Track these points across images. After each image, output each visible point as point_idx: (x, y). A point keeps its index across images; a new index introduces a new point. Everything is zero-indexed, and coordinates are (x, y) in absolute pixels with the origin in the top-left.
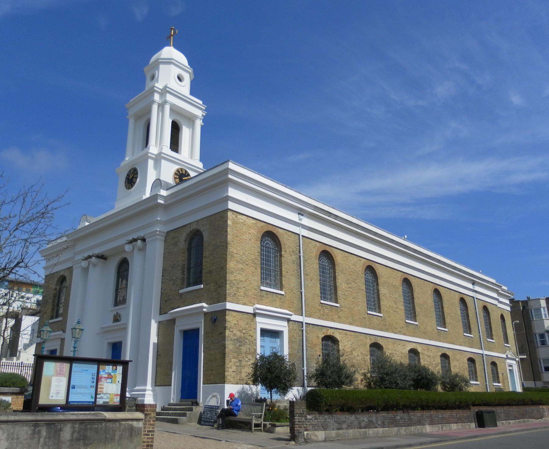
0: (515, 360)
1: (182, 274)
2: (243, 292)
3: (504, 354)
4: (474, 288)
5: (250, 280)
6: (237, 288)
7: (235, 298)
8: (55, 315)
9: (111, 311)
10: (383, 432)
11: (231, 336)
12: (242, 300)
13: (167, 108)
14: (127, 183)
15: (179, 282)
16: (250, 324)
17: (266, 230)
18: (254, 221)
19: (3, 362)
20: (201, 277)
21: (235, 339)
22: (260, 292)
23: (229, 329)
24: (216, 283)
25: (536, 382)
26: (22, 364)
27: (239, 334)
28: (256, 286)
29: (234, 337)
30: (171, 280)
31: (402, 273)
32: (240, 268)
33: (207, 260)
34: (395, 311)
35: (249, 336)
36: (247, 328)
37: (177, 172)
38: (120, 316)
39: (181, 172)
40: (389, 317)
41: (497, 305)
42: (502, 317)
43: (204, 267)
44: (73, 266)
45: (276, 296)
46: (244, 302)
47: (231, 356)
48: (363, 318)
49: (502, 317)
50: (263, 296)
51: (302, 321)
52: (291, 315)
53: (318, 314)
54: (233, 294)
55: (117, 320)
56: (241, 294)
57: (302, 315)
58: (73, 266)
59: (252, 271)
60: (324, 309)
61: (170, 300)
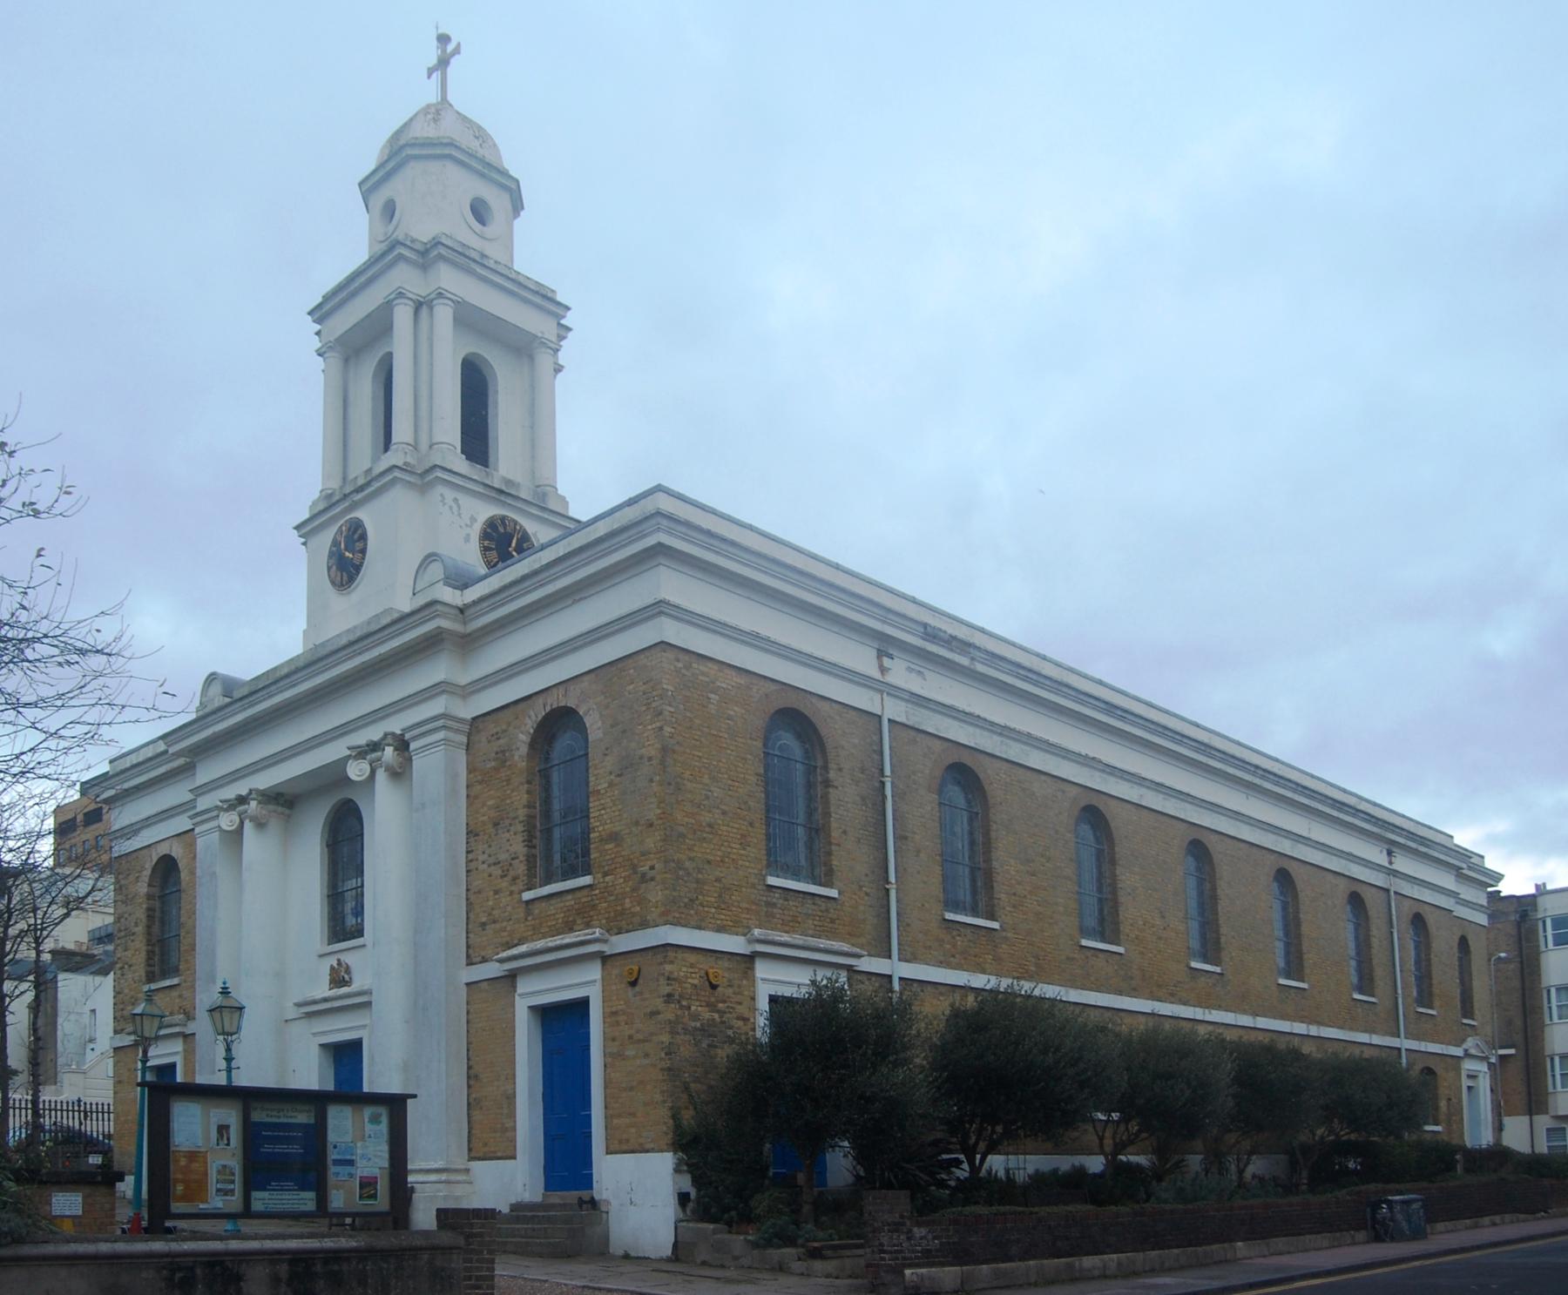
0: (1485, 1059)
1: (527, 846)
2: (716, 895)
3: (1459, 1046)
4: (1391, 863)
5: (734, 857)
6: (698, 881)
7: (692, 912)
8: (156, 969)
9: (321, 956)
10: (1119, 1264)
11: (686, 1020)
12: (714, 918)
13: (444, 315)
14: (334, 567)
15: (520, 868)
16: (739, 986)
17: (781, 704)
18: (742, 680)
19: (44, 1101)
20: (586, 853)
21: (695, 1029)
22: (766, 894)
23: (679, 1002)
24: (634, 868)
25: (1536, 1118)
26: (79, 1106)
27: (706, 1015)
28: (753, 876)
29: (693, 1024)
30: (495, 864)
31: (1412, 902)
32: (704, 824)
33: (602, 801)
34: (1160, 938)
35: (738, 1018)
36: (729, 997)
37: (489, 530)
38: (348, 970)
39: (501, 530)
40: (1142, 953)
41: (1452, 911)
42: (1463, 943)
43: (594, 823)
44: (193, 830)
45: (814, 904)
46: (719, 922)
47: (686, 1075)
48: (1068, 958)
49: (1463, 943)
50: (774, 905)
51: (888, 972)
52: (859, 956)
53: (936, 953)
54: (686, 900)
55: (340, 982)
56: (709, 899)
57: (890, 957)
58: (193, 830)
59: (741, 832)
60: (953, 938)
61: (494, 922)
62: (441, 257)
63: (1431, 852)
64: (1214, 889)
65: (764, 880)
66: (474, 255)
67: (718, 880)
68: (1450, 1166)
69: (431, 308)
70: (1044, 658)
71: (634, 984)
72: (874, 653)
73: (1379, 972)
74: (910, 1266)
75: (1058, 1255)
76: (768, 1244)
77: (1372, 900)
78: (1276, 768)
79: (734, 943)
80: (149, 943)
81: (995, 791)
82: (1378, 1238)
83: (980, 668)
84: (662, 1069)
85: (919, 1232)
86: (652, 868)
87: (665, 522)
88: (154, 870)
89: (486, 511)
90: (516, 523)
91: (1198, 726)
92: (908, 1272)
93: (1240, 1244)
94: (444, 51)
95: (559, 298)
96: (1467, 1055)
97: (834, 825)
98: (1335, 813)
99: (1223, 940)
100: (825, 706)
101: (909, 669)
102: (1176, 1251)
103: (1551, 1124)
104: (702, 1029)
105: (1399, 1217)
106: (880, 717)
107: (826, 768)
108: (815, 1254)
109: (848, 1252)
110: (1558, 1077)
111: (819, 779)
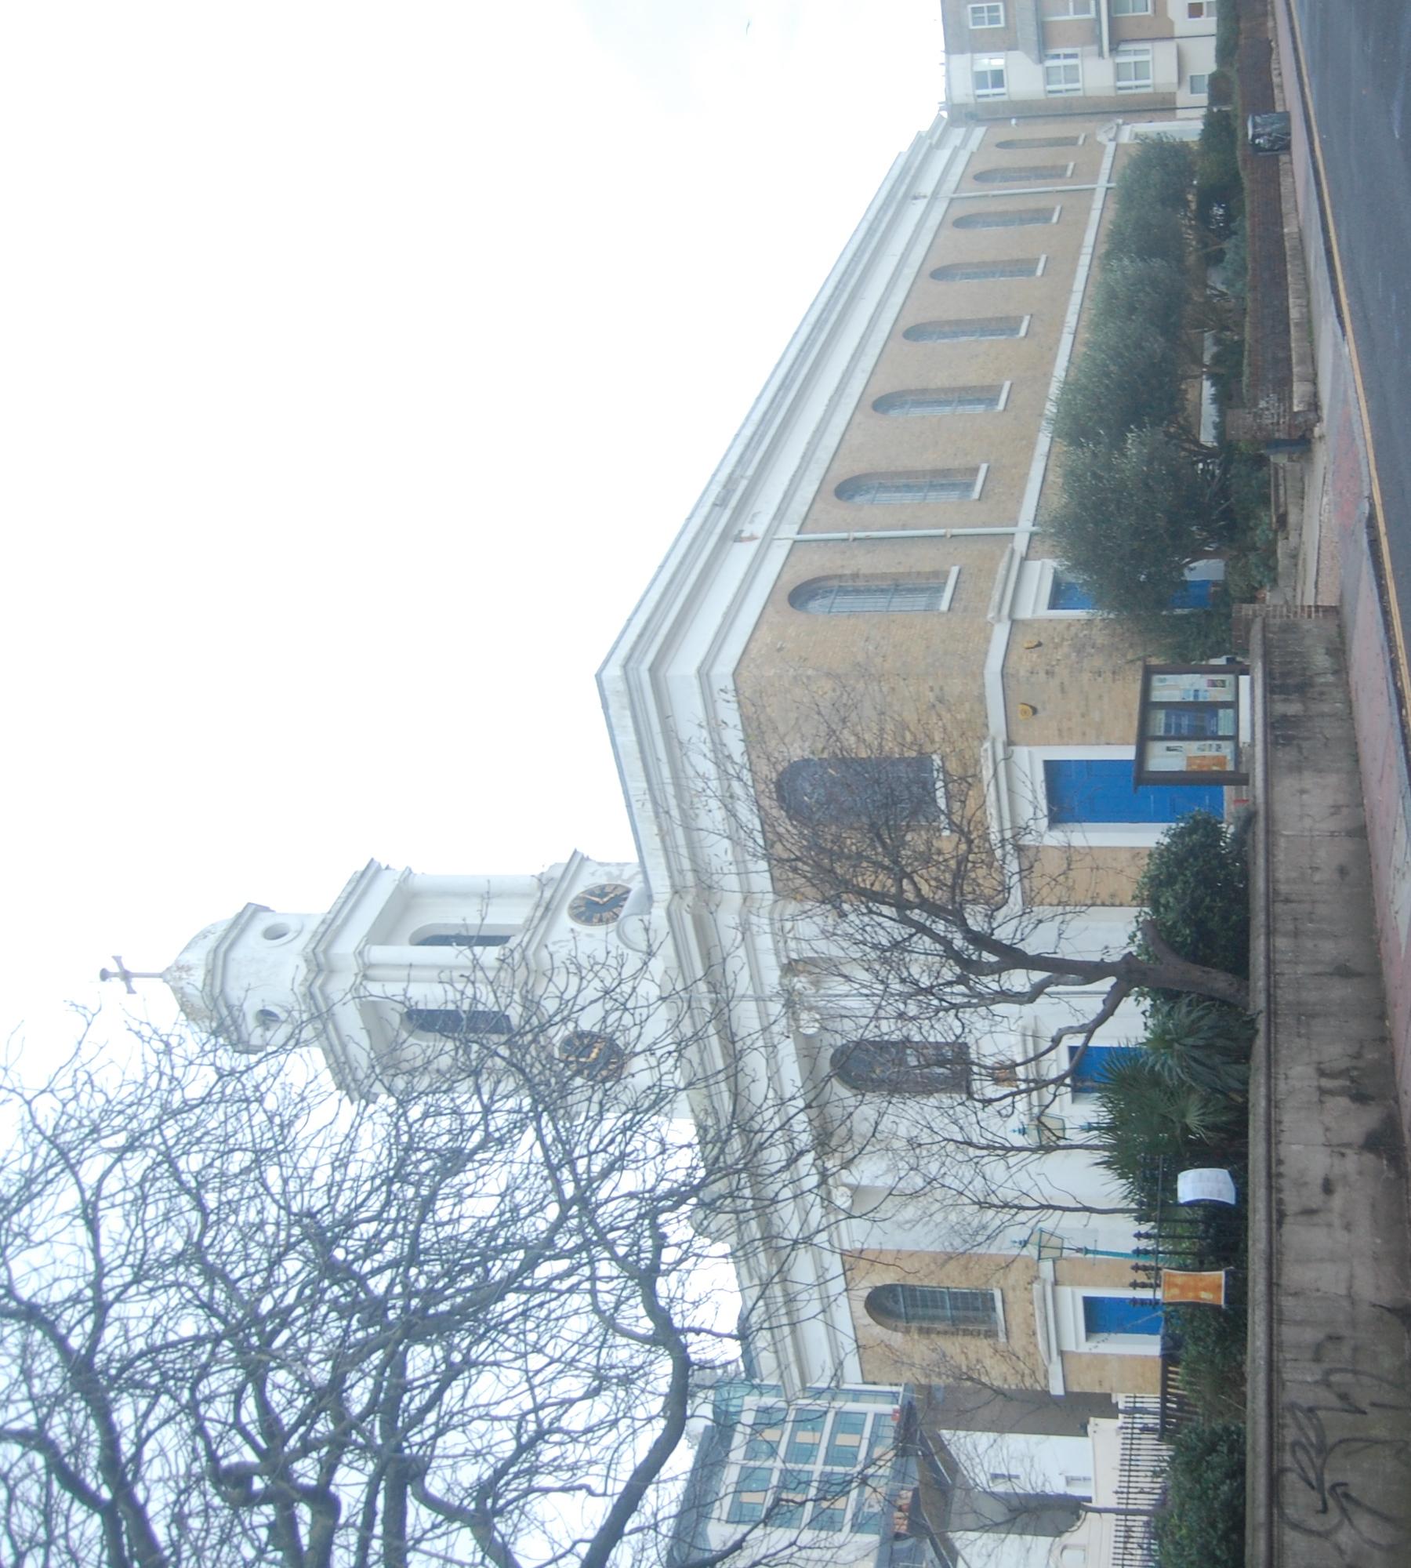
3: (1105, 146)
8: (983, 1328)
13: (378, 953)
52: (1013, 552)
62: (326, 952)
63: (917, 163)
64: (949, 323)
65: (943, 613)
66: (322, 929)
67: (943, 642)
68: (1226, 116)
69: (371, 966)
70: (737, 435)
71: (1035, 711)
72: (738, 545)
73: (1032, 204)
74: (1291, 406)
75: (1288, 332)
76: (1273, 569)
77: (959, 211)
78: (819, 306)
79: (1000, 634)
80: (955, 1333)
81: (860, 468)
82: (1287, 147)
83: (750, 472)
84: (1114, 680)
85: (1262, 404)
86: (932, 689)
87: (631, 664)
88: (879, 1323)
89: (565, 921)
90: (577, 898)
91: (796, 333)
92: (1296, 409)
93: (1286, 230)
94: (115, 975)
95: (362, 868)
96: (1114, 139)
97: (893, 570)
98: (878, 235)
99: (998, 315)
100: (785, 578)
101: (752, 522)
102: (1289, 266)
103: (1186, 88)
104: (1079, 652)
105: (1268, 130)
106: (795, 542)
107: (841, 577)
108: (1283, 520)
109: (1282, 500)
110: (1138, 83)
111: (850, 583)
